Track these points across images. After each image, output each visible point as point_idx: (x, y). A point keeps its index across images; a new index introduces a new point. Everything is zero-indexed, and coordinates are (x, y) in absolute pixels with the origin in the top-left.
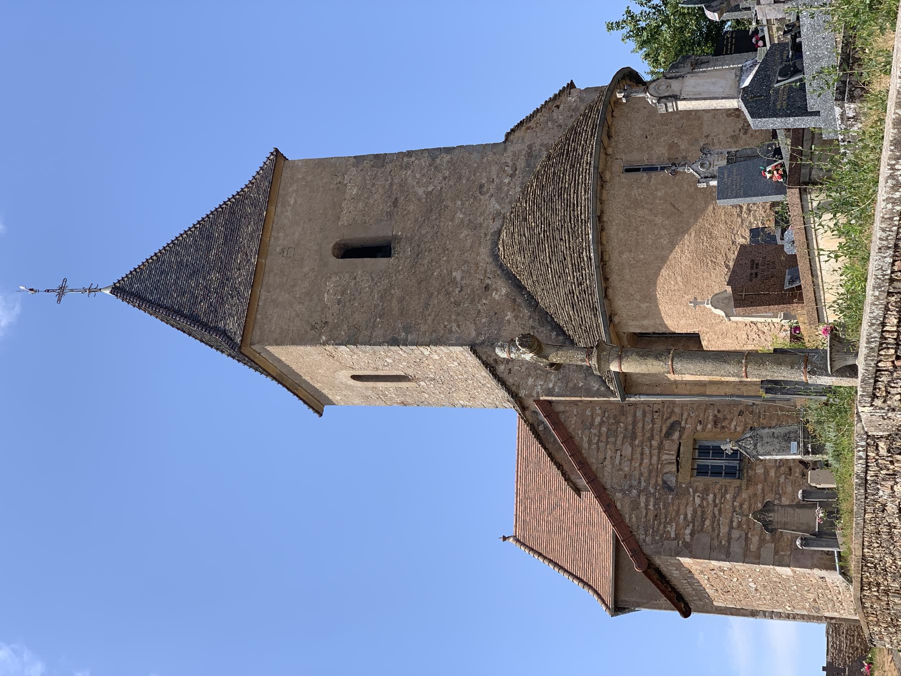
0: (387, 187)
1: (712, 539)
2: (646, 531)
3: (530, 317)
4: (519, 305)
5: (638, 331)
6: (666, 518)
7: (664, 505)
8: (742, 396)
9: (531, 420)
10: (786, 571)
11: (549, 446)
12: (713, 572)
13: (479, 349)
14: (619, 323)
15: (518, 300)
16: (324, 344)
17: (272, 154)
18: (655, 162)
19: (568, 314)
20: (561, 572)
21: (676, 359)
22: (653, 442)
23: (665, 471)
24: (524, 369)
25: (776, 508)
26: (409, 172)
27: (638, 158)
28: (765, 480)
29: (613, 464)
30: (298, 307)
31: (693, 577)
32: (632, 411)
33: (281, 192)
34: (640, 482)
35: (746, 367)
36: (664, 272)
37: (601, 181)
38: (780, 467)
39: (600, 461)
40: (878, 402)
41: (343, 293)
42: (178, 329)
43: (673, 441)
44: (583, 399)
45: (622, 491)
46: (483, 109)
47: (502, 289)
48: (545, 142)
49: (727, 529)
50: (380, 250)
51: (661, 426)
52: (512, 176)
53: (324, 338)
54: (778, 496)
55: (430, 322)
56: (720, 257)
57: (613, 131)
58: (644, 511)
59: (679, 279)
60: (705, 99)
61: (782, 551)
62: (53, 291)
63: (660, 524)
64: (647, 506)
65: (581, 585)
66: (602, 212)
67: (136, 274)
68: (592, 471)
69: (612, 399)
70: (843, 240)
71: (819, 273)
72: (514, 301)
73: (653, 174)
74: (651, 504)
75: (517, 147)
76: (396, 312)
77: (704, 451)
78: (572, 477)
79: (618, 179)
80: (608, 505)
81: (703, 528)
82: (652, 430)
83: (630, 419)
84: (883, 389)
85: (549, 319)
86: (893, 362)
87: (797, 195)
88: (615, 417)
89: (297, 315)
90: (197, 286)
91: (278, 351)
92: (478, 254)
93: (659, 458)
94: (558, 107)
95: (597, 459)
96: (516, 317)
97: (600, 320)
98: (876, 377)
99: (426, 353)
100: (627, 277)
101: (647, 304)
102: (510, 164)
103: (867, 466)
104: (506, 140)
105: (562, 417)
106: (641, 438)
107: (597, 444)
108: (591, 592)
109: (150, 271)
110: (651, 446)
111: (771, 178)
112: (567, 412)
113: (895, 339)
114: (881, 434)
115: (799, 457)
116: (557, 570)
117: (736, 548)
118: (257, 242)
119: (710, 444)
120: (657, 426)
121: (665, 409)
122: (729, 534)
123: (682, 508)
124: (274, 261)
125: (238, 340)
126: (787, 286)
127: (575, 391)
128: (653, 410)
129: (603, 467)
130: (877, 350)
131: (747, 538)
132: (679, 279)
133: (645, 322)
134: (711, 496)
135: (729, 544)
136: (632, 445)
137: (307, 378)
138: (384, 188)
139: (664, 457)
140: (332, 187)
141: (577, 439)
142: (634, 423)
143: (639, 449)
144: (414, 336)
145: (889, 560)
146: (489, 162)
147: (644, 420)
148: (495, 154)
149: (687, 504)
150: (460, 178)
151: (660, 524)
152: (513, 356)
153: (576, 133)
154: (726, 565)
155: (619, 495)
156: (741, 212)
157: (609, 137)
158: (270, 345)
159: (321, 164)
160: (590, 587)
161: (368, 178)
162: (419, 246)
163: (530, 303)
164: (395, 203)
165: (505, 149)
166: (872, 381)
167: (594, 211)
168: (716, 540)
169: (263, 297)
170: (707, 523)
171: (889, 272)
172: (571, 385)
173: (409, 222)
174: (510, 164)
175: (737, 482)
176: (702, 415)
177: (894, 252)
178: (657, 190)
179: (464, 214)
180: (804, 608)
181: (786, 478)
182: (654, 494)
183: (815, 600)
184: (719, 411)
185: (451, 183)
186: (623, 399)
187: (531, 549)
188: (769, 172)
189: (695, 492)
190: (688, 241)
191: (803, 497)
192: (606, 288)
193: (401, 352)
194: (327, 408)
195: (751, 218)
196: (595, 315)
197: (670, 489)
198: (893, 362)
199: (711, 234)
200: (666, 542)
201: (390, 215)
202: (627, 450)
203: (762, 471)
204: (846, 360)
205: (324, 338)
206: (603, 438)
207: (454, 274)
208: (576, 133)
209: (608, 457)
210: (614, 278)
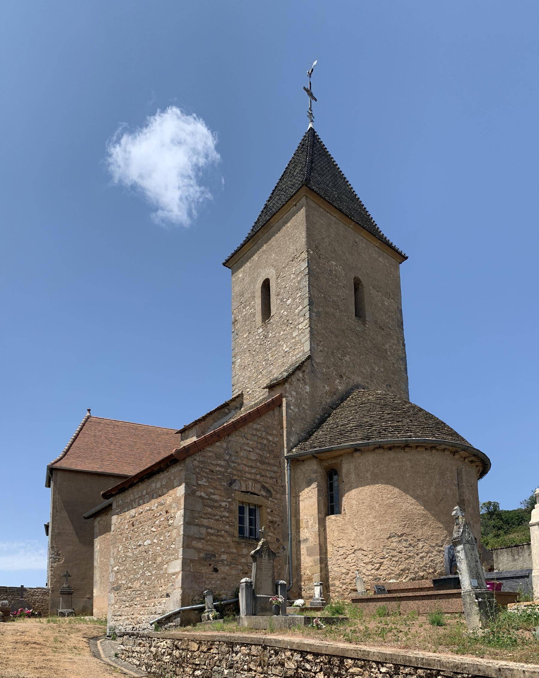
1: (199, 512)
2: (202, 462)
4: (332, 397)
6: (211, 479)
8: (291, 542)
15: (335, 396)
16: (307, 251)
23: (242, 482)
25: (271, 561)
28: (239, 555)
29: (244, 444)
32: (276, 464)
34: (233, 462)
36: (397, 490)
38: (248, 566)
39: (246, 435)
43: (260, 491)
45: (227, 449)
49: (206, 524)
50: (359, 313)
54: (229, 563)
56: (409, 530)
58: (214, 463)
59: (392, 501)
61: (193, 565)
63: (207, 473)
64: (217, 465)
68: (239, 428)
69: (285, 450)
72: (335, 394)
74: (220, 469)
77: (252, 512)
80: (219, 435)
82: (266, 476)
83: (272, 461)
85: (326, 415)
88: (272, 451)
89: (323, 239)
91: (301, 216)
93: (249, 479)
96: (326, 393)
101: (369, 477)
105: (271, 413)
106: (261, 467)
107: (256, 435)
108: (61, 456)
112: (274, 416)
117: (194, 530)
120: (268, 480)
121: (278, 487)
131: (201, 539)
132: (392, 501)
134: (227, 515)
136: (256, 460)
137: (265, 247)
141: (259, 421)
142: (269, 464)
143: (254, 465)
144: (315, 318)
147: (272, 471)
149: (221, 496)
151: (207, 473)
155: (225, 445)
156: (439, 546)
160: (64, 456)
161: (393, 314)
163: (334, 404)
168: (198, 515)
170: (209, 510)
172: (293, 422)
175: (237, 534)
178: (450, 489)
181: (241, 570)
182: (226, 472)
184: (278, 525)
186: (287, 458)
187: (84, 425)
189: (229, 502)
190: (420, 509)
191: (281, 585)
193: (300, 308)
195: (435, 553)
197: (231, 484)
199: (424, 524)
200: (194, 476)
201: (376, 323)
202: (253, 457)
207: (348, 356)
209: (249, 441)
210: (391, 454)
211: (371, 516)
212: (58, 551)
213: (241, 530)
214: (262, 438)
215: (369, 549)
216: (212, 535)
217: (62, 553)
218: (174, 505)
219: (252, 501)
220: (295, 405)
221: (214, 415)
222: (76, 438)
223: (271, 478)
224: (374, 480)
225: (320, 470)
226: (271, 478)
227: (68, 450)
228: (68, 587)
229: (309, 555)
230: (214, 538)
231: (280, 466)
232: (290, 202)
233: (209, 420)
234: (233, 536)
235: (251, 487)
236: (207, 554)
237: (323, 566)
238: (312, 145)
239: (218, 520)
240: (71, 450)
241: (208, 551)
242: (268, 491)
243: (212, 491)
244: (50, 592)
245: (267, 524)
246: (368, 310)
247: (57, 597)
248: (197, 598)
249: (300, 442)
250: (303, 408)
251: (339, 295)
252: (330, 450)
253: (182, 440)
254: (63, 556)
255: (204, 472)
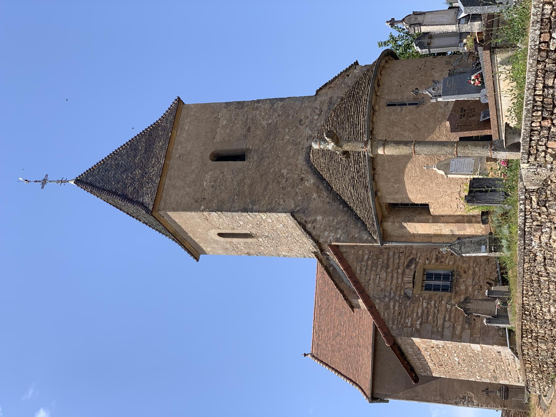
0: (244, 120)
3: (327, 197)
4: (321, 190)
5: (392, 202)
6: (405, 314)
7: (405, 307)
9: (325, 264)
10: (477, 347)
11: (336, 280)
12: (433, 349)
13: (296, 215)
14: (381, 196)
16: (203, 211)
17: (176, 100)
18: (405, 100)
19: (351, 192)
20: (339, 376)
21: (416, 145)
22: (399, 270)
23: (406, 287)
24: (322, 226)
25: (472, 301)
26: (258, 112)
27: (395, 98)
29: (374, 283)
30: (188, 190)
31: (420, 354)
33: (180, 123)
34: (390, 294)
35: (457, 148)
36: (409, 165)
37: (373, 110)
38: (475, 285)
39: (367, 281)
40: (532, 159)
41: (215, 181)
42: (114, 206)
43: (411, 269)
44: (358, 244)
46: (303, 75)
47: (311, 180)
48: (340, 96)
49: (442, 321)
50: (240, 157)
51: (404, 261)
52: (319, 115)
53: (203, 207)
55: (267, 199)
57: (381, 82)
59: (417, 169)
60: (437, 25)
61: (475, 334)
62: (39, 181)
63: (401, 318)
64: (394, 307)
65: (351, 383)
66: (373, 129)
67: (90, 172)
68: (362, 287)
69: (375, 244)
70: (515, 84)
71: (500, 102)
72: (318, 187)
73: (404, 107)
74: (397, 306)
75: (323, 98)
76: (247, 193)
77: (429, 276)
78: (349, 298)
79: (383, 109)
80: (371, 307)
81: (427, 320)
82: (399, 263)
83: (385, 257)
84: (535, 147)
85: (339, 198)
86: (540, 122)
87: (489, 55)
89: (187, 194)
90: (127, 177)
91: (174, 215)
92: (297, 160)
93: (402, 280)
94: (348, 76)
95: (365, 280)
96: (319, 197)
97: (370, 194)
98: (531, 136)
99: (264, 218)
100: (387, 168)
102: (319, 108)
103: (526, 218)
104: (317, 94)
105: (345, 255)
107: (365, 271)
108: (357, 388)
109: (99, 170)
110: (398, 273)
111: (474, 84)
113: (541, 102)
114: (533, 188)
115: (486, 254)
116: (337, 374)
117: (447, 332)
118: (164, 151)
119: (433, 272)
120: (402, 261)
122: (443, 325)
123: (415, 309)
124: (174, 162)
125: (151, 208)
126: (482, 119)
127: (353, 239)
128: (399, 252)
129: (369, 285)
130: (531, 111)
131: (454, 327)
132: (417, 169)
133: (397, 196)
134: (433, 302)
135: (443, 330)
136: (386, 272)
137: (191, 235)
138: (242, 121)
139: (405, 279)
140: (211, 120)
141: (353, 268)
142: (388, 259)
144: (257, 207)
145: (538, 307)
146: (306, 107)
148: (309, 102)
149: (419, 306)
150: (288, 116)
151: (401, 318)
152: (322, 147)
153: (359, 84)
154: (441, 343)
155: (377, 301)
157: (379, 86)
158: (170, 211)
159: (205, 106)
160: (357, 385)
162: (262, 154)
163: (328, 189)
164: (249, 130)
165: (316, 100)
166: (528, 139)
167: (368, 127)
169: (167, 183)
170: (430, 318)
171: (538, 43)
172: (350, 236)
173: (257, 141)
174: (319, 108)
175: (448, 294)
176: (429, 255)
177: (541, 25)
179: (290, 136)
180: (487, 377)
181: (478, 292)
183: (494, 371)
185: (283, 118)
186: (382, 244)
187: (321, 362)
188: (473, 80)
189: (423, 299)
191: (488, 294)
192: (374, 175)
193: (249, 217)
194: (202, 257)
196: (367, 191)
197: (409, 298)
198: (540, 122)
200: (405, 329)
201: (245, 136)
202: (383, 275)
203: (464, 287)
204: (514, 139)
205: (203, 207)
206: (369, 268)
207: (282, 171)
208: (359, 84)
211: (431, 185)
212: (460, 398)
213: (445, 289)
214: (367, 266)
215: (459, 187)
216: (450, 316)
217: (462, 394)
218: (428, 344)
219: (421, 279)
220: (336, 233)
221: (337, 282)
222: (336, 371)
223: (399, 258)
224: (402, 182)
225: (391, 219)
226: (399, 258)
227: (351, 380)
228: (500, 391)
229: (465, 230)
230: (453, 314)
231: (388, 248)
232: (161, 221)
233: (342, 286)
234: (450, 297)
235: (408, 279)
236: (466, 322)
237: (474, 219)
238: (88, 182)
239: (438, 311)
240: (350, 377)
241: (463, 320)
242: (411, 262)
243: (415, 314)
244: (506, 409)
245: (438, 264)
246: (235, 146)
247: (511, 402)
248: (501, 333)
249: (366, 229)
250: (337, 223)
251: (231, 178)
252: (376, 215)
253: (360, 308)
254: (465, 393)
255: (401, 321)
